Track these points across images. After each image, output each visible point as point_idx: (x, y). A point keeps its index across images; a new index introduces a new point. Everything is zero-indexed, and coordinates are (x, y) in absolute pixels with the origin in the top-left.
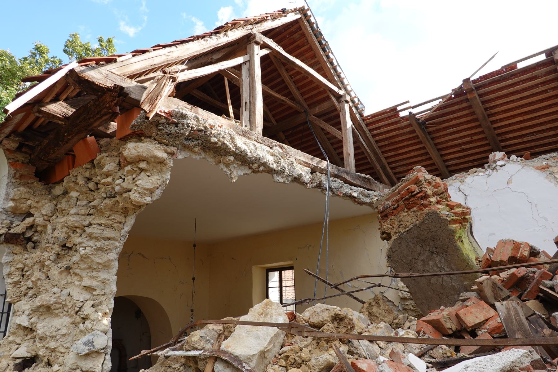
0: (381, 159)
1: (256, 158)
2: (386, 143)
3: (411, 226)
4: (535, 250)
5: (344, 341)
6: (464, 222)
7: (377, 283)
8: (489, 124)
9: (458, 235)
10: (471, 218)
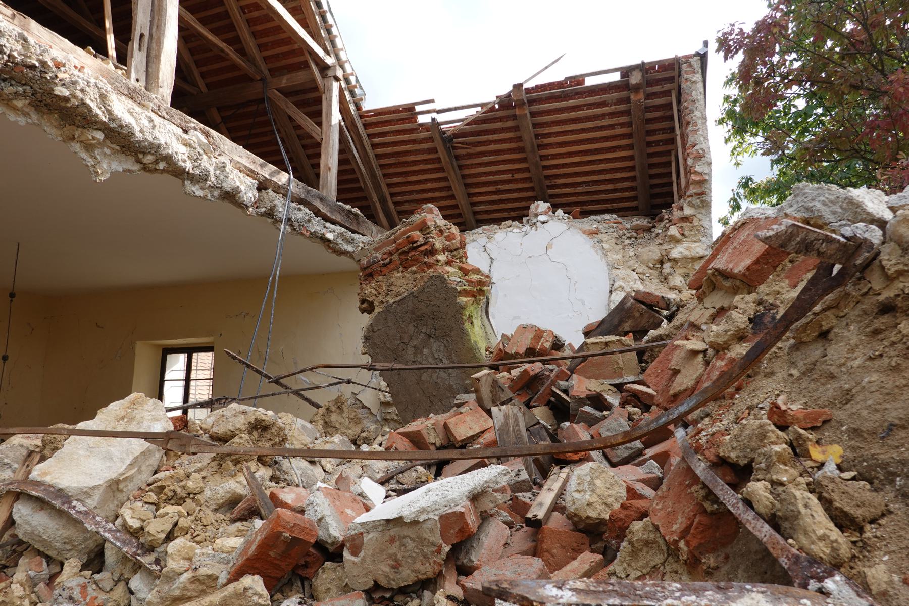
0: (380, 186)
1: (151, 143)
2: (392, 160)
3: (405, 294)
4: (559, 341)
5: (267, 462)
6: (480, 295)
7: (345, 378)
8: (538, 159)
9: (467, 313)
10: (489, 292)
